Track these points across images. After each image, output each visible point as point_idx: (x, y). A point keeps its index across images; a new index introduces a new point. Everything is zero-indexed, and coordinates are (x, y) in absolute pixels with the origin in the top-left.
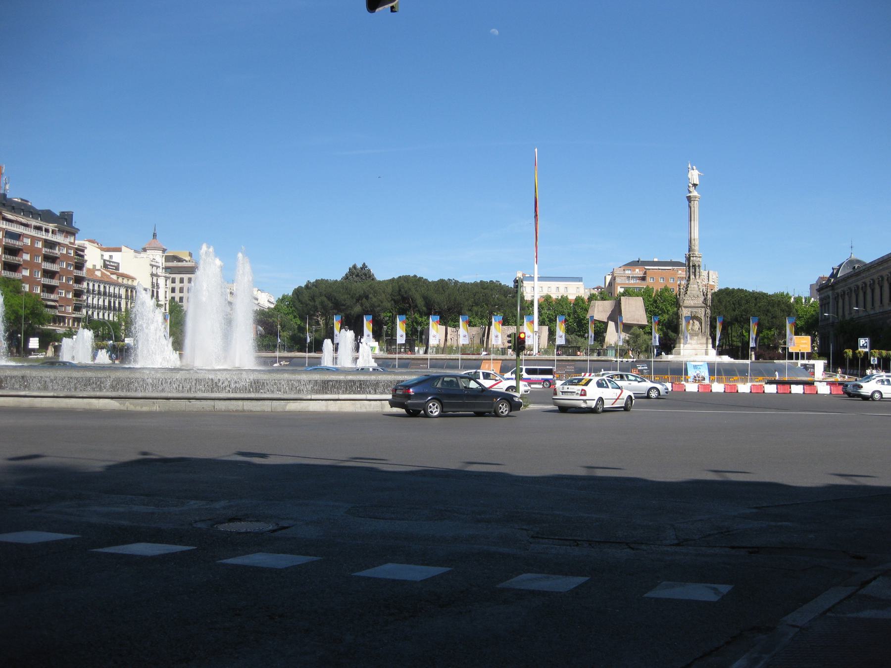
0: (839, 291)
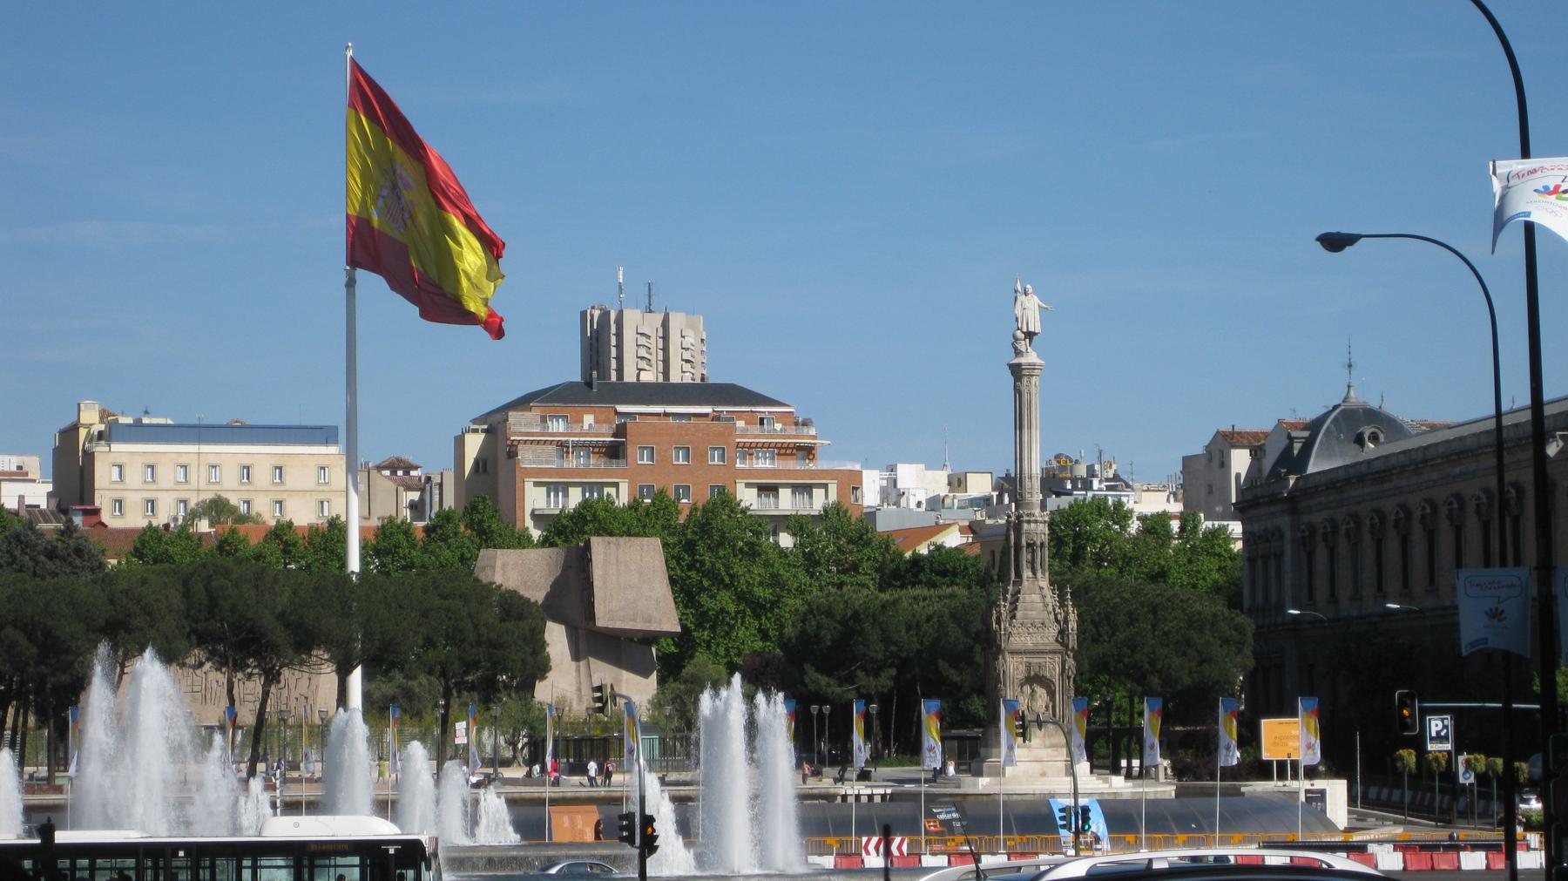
0: (1318, 518)
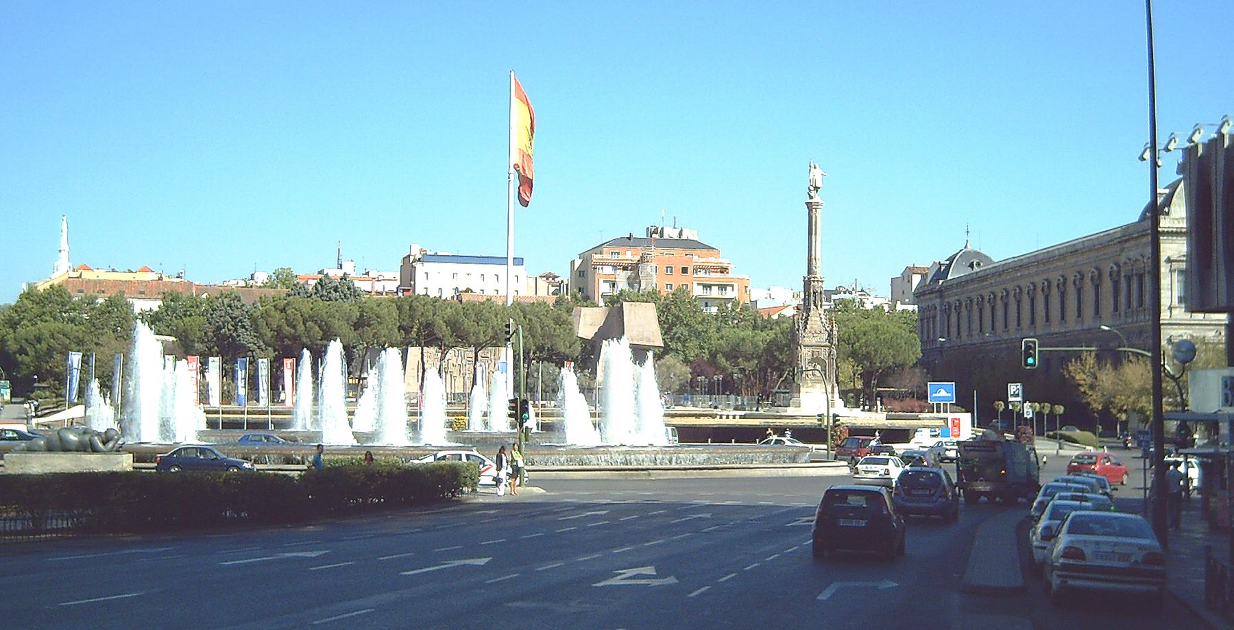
0: (952, 300)
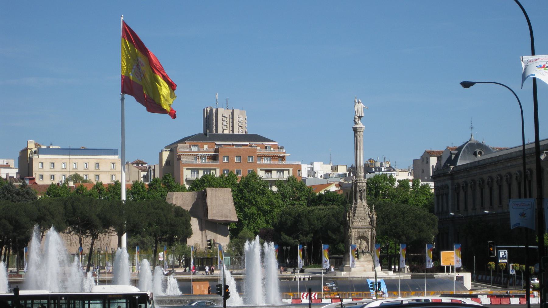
0: (461, 181)
